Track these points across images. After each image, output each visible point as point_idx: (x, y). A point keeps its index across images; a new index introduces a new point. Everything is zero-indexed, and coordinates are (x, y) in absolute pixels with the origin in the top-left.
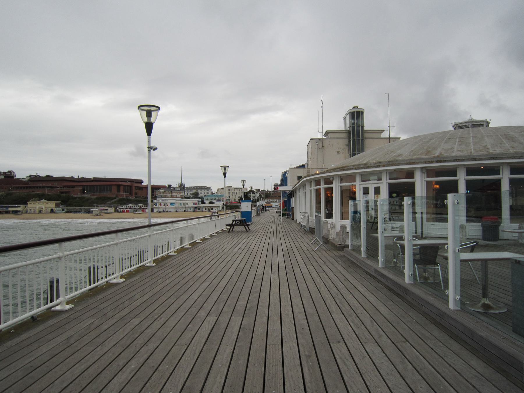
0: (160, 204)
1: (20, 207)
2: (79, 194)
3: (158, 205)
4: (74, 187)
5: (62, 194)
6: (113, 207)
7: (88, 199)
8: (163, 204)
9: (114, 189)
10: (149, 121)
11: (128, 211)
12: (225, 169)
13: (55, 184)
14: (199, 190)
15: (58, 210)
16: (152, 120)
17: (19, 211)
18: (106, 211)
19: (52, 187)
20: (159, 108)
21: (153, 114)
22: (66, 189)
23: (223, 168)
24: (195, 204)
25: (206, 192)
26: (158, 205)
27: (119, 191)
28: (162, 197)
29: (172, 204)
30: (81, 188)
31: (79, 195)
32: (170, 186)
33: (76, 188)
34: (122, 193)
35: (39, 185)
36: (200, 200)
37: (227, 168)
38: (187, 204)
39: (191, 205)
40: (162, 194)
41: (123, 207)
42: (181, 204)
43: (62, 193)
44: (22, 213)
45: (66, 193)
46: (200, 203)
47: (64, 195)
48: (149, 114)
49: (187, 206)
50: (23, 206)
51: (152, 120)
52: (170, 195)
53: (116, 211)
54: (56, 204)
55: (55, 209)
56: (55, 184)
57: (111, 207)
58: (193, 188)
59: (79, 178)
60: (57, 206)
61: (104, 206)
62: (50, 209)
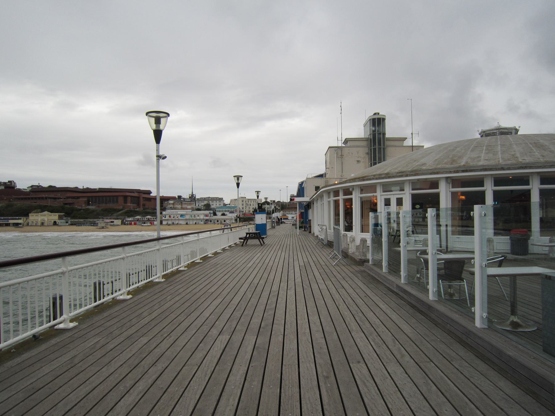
0: (170, 216)
1: (21, 219)
2: (83, 205)
3: (167, 217)
4: (78, 198)
5: (66, 206)
6: (120, 219)
7: (93, 211)
8: (172, 216)
9: (121, 200)
10: (157, 129)
11: (135, 224)
12: (238, 179)
13: (59, 195)
14: (210, 202)
15: (61, 223)
16: (161, 127)
17: (20, 224)
18: (112, 224)
19: (55, 198)
20: (168, 115)
21: (163, 120)
22: (70, 201)
23: (236, 178)
24: (207, 216)
25: (218, 203)
26: (167, 217)
27: (125, 202)
28: (171, 208)
29: (182, 216)
30: (85, 199)
31: (84, 207)
32: (180, 197)
33: (81, 199)
34: (129, 205)
35: (41, 196)
36: (212, 212)
37: (240, 178)
38: (198, 216)
39: (202, 217)
40: (171, 206)
41: (130, 219)
42: (191, 216)
43: (66, 204)
44: (23, 225)
45: (70, 204)
46: (212, 215)
47: (68, 206)
48: (158, 121)
49: (198, 218)
50: (25, 219)
51: (161, 127)
52: (180, 206)
53: (123, 223)
54: (59, 216)
55: (58, 221)
56: (59, 195)
57: (118, 219)
58: (205, 199)
59: (83, 189)
60: (60, 218)
61: (110, 219)
62: (53, 221)
